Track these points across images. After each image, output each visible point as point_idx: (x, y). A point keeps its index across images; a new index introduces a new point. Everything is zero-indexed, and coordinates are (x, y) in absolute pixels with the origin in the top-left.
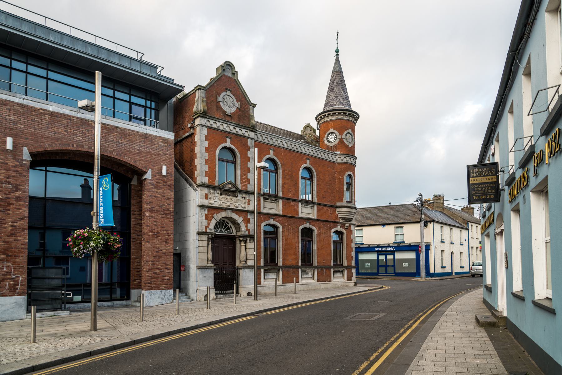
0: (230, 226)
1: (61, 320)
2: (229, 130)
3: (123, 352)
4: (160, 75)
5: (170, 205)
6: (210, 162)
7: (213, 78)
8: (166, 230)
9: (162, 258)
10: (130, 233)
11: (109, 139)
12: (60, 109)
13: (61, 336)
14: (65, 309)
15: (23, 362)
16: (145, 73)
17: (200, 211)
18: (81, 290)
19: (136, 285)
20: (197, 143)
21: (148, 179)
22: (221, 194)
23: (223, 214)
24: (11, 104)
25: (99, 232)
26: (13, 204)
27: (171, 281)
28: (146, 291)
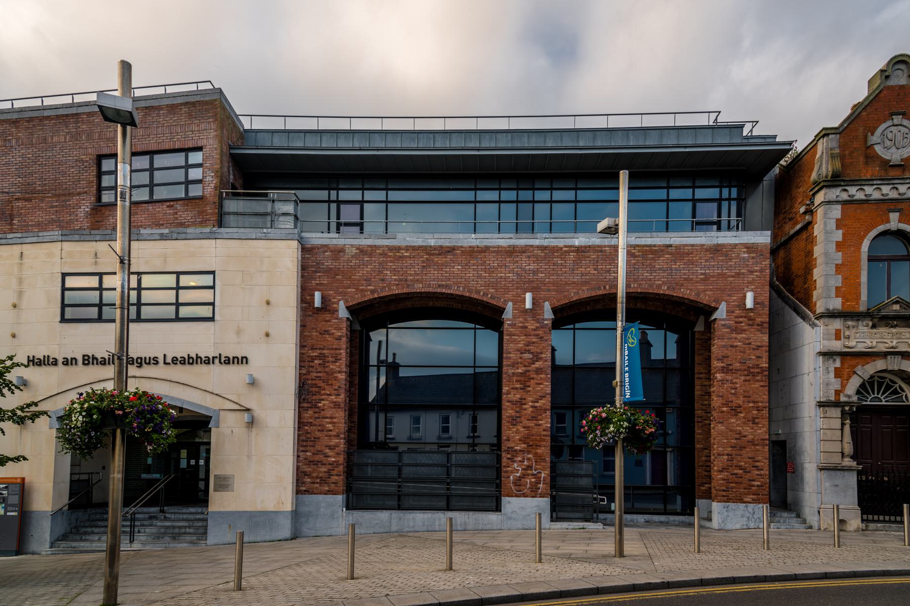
0: (900, 386)
1: (589, 535)
2: (863, 197)
3: (644, 598)
4: (753, 137)
5: (760, 357)
6: (848, 269)
7: (859, 103)
8: (754, 402)
9: (747, 449)
10: (693, 410)
11: (656, 266)
12: (588, 240)
13: (573, 559)
14: (596, 521)
15: (514, 587)
16: (722, 143)
17: (823, 363)
18: (630, 494)
19: (704, 493)
20: (818, 238)
21: (720, 320)
22: (874, 327)
23: (880, 365)
24: (531, 249)
25: (624, 410)
26: (533, 379)
27: (765, 490)
28: (718, 504)
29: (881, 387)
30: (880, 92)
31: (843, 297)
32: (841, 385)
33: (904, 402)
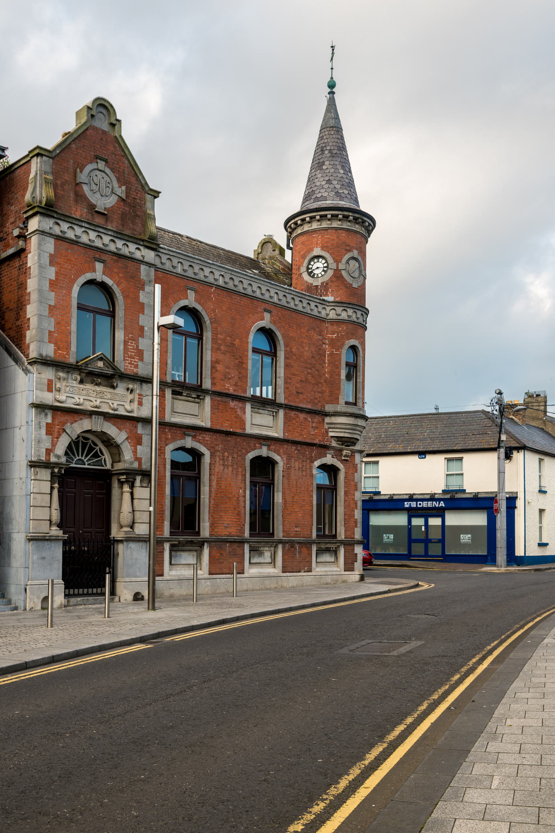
0: (100, 449)
7: (69, 132)
17: (35, 416)
22: (81, 382)
23: (86, 424)
29: (85, 449)
30: (87, 129)
31: (56, 344)
32: (52, 443)
33: (103, 466)
